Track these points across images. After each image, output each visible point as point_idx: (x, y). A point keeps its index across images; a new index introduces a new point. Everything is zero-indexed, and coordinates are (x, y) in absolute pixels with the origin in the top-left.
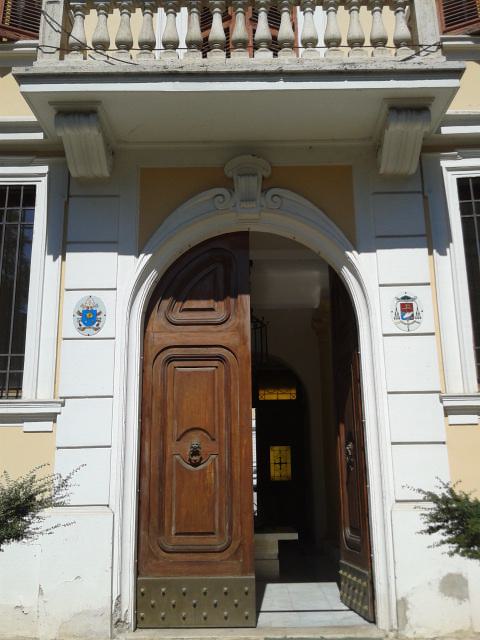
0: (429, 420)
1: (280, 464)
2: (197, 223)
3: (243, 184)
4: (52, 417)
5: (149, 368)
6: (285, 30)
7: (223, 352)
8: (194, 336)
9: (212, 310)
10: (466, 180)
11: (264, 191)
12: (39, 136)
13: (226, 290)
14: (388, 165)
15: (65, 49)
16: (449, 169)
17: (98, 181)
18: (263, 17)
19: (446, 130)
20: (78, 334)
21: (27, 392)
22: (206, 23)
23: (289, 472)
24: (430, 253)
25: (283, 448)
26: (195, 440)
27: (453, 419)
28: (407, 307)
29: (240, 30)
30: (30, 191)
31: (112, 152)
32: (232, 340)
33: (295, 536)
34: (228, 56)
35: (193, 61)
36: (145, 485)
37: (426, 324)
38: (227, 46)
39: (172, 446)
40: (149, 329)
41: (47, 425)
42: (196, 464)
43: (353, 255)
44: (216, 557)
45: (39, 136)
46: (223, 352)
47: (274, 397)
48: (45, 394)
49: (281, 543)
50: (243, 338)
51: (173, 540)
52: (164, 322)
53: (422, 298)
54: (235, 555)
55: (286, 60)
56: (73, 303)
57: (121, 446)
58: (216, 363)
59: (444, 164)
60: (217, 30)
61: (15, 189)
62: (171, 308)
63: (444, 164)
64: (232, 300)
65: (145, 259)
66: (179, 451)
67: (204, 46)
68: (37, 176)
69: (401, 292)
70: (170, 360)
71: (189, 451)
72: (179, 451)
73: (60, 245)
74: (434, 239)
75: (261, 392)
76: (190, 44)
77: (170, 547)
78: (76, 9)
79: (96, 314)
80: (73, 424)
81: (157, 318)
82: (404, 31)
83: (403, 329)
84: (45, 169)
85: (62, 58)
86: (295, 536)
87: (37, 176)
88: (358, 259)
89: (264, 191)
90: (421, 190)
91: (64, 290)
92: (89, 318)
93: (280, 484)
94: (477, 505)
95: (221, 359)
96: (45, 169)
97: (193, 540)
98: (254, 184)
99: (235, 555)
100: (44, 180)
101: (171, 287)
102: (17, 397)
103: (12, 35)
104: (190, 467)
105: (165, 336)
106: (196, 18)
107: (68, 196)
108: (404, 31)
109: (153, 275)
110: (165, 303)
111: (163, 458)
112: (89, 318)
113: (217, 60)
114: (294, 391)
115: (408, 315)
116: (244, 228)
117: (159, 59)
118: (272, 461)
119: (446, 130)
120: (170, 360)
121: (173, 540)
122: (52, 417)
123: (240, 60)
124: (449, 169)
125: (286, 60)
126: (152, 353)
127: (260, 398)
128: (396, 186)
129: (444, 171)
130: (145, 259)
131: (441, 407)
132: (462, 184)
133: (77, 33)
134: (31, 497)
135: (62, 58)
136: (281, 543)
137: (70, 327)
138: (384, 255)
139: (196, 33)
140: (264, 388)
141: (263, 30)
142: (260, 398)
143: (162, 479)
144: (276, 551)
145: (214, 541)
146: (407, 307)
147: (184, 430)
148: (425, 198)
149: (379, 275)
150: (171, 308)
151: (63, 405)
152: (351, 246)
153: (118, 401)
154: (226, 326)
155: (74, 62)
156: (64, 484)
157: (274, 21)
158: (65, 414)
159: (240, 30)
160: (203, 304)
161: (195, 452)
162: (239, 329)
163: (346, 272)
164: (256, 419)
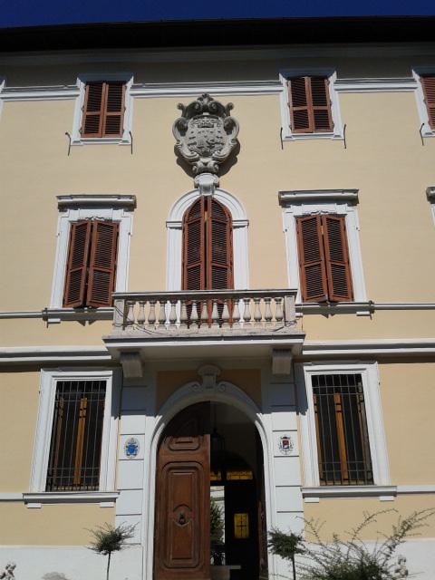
0: (294, 500)
1: (241, 526)
2: (185, 398)
3: (206, 379)
4: (114, 500)
5: (160, 474)
6: (226, 314)
7: (196, 465)
8: (182, 456)
9: (191, 442)
11: (217, 382)
12: (109, 357)
13: (197, 432)
14: (276, 370)
15: (126, 324)
16: (308, 371)
17: (138, 379)
18: (215, 307)
19: (305, 353)
20: (126, 458)
21: (101, 488)
23: (247, 533)
24: (298, 414)
25: (243, 515)
26: (182, 511)
27: (307, 499)
28: (286, 442)
29: (204, 315)
30: (104, 384)
31: (144, 365)
32: (200, 458)
33: (238, 567)
35: (180, 330)
36: (157, 536)
38: (199, 322)
39: (171, 514)
40: (160, 453)
41: (111, 504)
42: (182, 523)
43: (260, 415)
44: (191, 570)
45: (109, 357)
46: (196, 465)
47: (237, 478)
48: (110, 488)
49: (232, 571)
50: (207, 458)
51: (171, 562)
52: (167, 449)
53: (293, 438)
54: (201, 570)
55: (226, 330)
56: (124, 441)
59: (305, 368)
60: (194, 315)
61: (96, 383)
62: (171, 441)
63: (305, 368)
64: (201, 437)
65: (159, 418)
66: (174, 517)
67: (188, 322)
68: (107, 376)
69: (283, 434)
70: (170, 469)
71: (179, 516)
72: (174, 517)
73: (118, 412)
74: (300, 408)
75: (228, 474)
76: (182, 321)
77: (170, 566)
78: (130, 304)
80: (123, 503)
81: (164, 446)
83: (283, 453)
84: (111, 372)
85: (124, 329)
86: (238, 567)
87: (107, 376)
88: (263, 417)
89: (217, 382)
90: (292, 381)
91: (120, 435)
92: (132, 449)
93: (242, 540)
95: (195, 468)
96: (111, 372)
97: (181, 562)
98: (212, 379)
99: (201, 570)
100: (111, 378)
101: (170, 432)
102: (95, 490)
103: (96, 305)
104: (179, 525)
105: (165, 458)
106: (184, 308)
107: (122, 386)
108: (280, 314)
109: (163, 425)
110: (168, 439)
111: (166, 522)
112: (132, 449)
113: (194, 328)
114: (251, 473)
115: (286, 446)
116: (208, 400)
117: (168, 330)
118: (235, 524)
119: (305, 353)
121: (171, 562)
122: (114, 500)
123: (204, 330)
124: (308, 371)
125: (226, 330)
126: (161, 466)
127: (228, 478)
128: (281, 380)
129: (305, 373)
130: (159, 418)
131: (301, 493)
132: (314, 378)
133: (130, 317)
134: (120, 534)
135: (124, 329)
136: (232, 571)
138: (274, 415)
140: (231, 470)
141: (215, 314)
142: (228, 478)
143: (166, 532)
144: (228, 577)
145: (190, 562)
146: (286, 442)
147: (177, 505)
148: (295, 386)
149: (273, 425)
150: (171, 441)
151: (119, 493)
152: (257, 409)
153: (145, 491)
154: (199, 450)
155: (131, 332)
156: (133, 529)
157: (231, 310)
158: (120, 498)
159: (204, 315)
160: (187, 439)
161: (182, 517)
162: (205, 452)
163: (257, 423)
164: (240, 480)
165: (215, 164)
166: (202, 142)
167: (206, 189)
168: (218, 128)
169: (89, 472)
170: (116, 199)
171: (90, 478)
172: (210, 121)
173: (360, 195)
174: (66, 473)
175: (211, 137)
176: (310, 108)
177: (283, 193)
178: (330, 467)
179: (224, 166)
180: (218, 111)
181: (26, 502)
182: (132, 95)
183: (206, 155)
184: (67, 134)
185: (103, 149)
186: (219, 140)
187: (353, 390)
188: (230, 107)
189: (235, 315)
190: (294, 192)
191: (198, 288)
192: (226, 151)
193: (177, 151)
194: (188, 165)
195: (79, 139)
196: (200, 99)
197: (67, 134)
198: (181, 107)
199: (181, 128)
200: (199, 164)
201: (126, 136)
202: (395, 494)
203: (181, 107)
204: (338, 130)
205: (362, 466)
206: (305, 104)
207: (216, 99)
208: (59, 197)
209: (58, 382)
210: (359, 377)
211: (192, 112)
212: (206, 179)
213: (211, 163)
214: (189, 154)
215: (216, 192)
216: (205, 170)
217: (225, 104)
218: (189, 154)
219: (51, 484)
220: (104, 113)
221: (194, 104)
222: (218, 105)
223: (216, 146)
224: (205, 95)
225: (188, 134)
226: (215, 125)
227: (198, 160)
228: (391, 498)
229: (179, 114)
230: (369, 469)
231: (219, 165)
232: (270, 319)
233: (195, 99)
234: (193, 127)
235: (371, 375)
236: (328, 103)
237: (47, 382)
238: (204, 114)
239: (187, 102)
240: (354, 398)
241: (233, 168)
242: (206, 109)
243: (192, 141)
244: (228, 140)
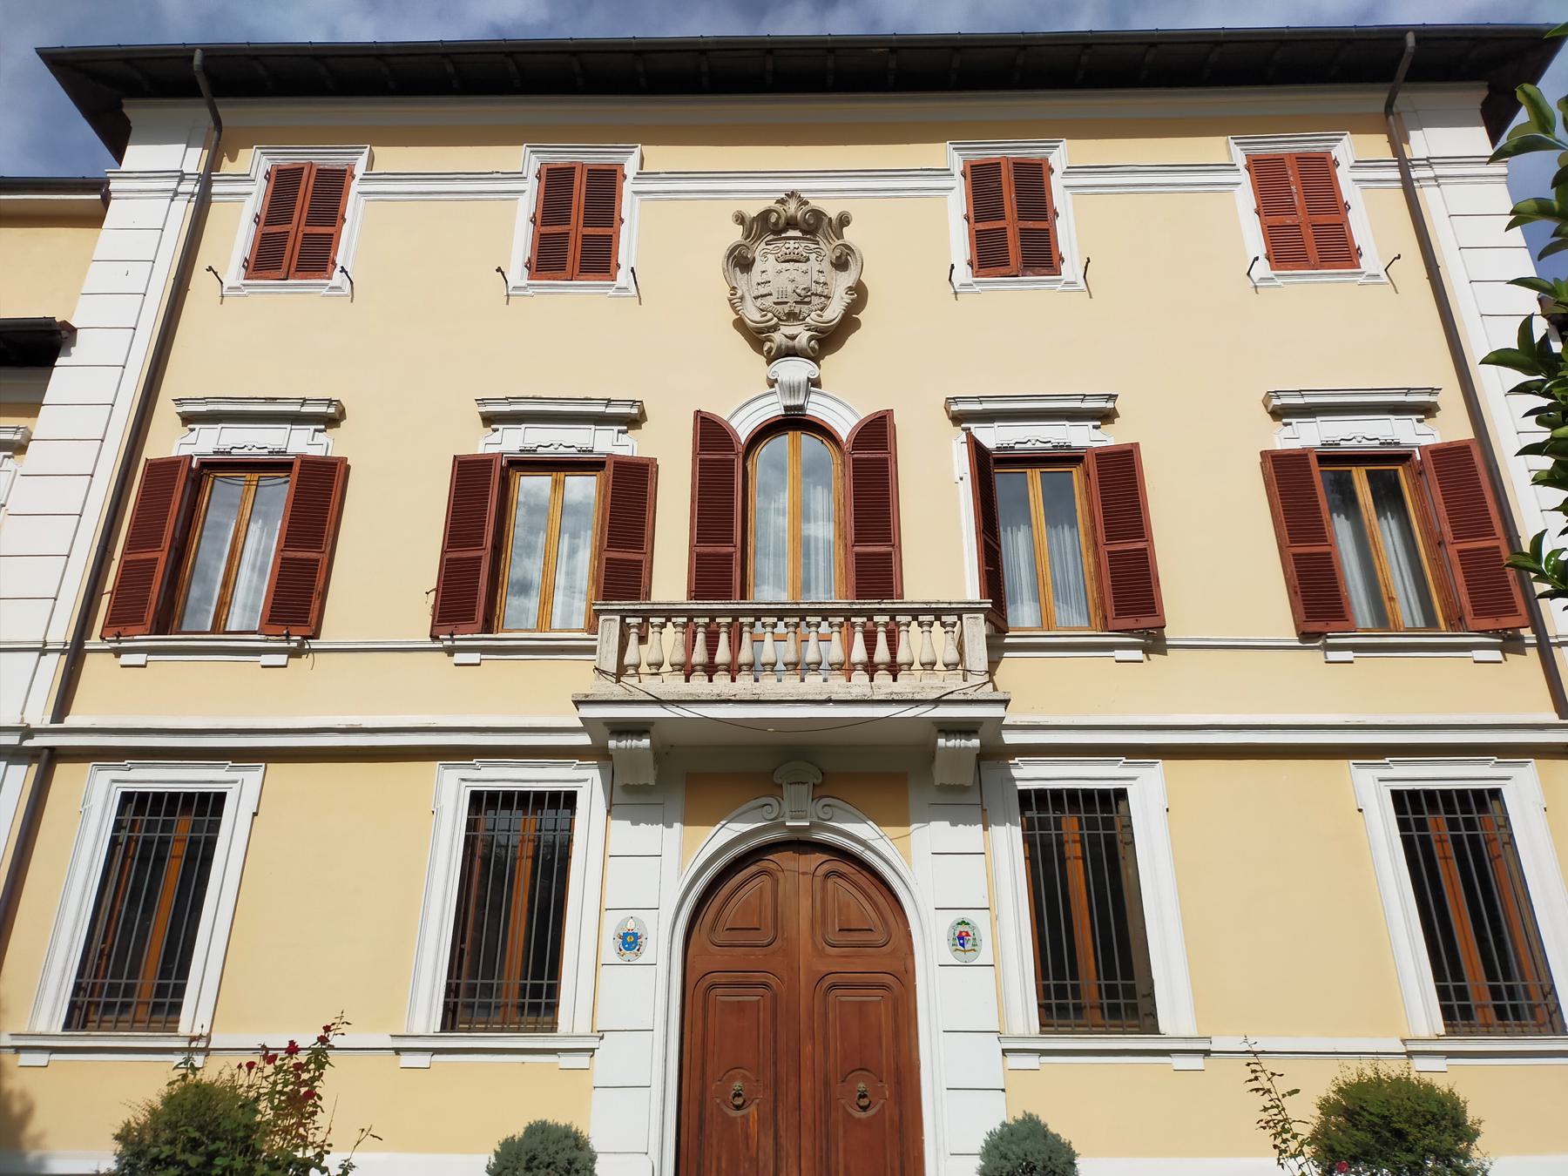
0: (984, 1061)
7: (888, 979)
10: (1401, 792)
18: (859, 638)
22: (690, 647)
27: (1015, 1061)
28: (963, 939)
34: (733, 680)
35: (673, 685)
37: (985, 956)
41: (581, 1061)
56: (613, 924)
57: (660, 1088)
58: (761, 991)
67: (687, 670)
70: (833, 987)
79: (636, 937)
82: (953, 656)
92: (630, 942)
94: (592, 1171)
95: (884, 986)
108: (953, 656)
112: (630, 942)
113: (722, 684)
120: (833, 987)
123: (813, 685)
137: (610, 951)
139: (679, 657)
157: (735, 645)
158: (603, 1048)
165: (811, 339)
166: (783, 293)
167: (792, 390)
168: (817, 267)
169: (536, 991)
170: (601, 409)
171: (537, 1001)
172: (801, 247)
173: (1119, 405)
174: (487, 990)
175: (804, 282)
176: (1011, 223)
177: (955, 400)
178: (1061, 992)
179: (828, 340)
180: (813, 225)
181: (398, 1051)
182: (636, 193)
183: (792, 316)
184: (499, 270)
185: (575, 299)
186: (819, 289)
187: (1109, 824)
188: (844, 220)
189: (902, 657)
190: (980, 399)
191: (727, 596)
192: (834, 312)
193: (740, 324)
194: (756, 337)
195: (524, 282)
196: (781, 202)
197: (499, 270)
198: (740, 219)
199: (741, 261)
200: (778, 337)
201: (623, 277)
202: (1207, 1053)
203: (740, 219)
204: (1071, 269)
205: (1130, 992)
206: (1002, 218)
207: (814, 204)
208: (482, 401)
209: (473, 793)
210: (1121, 794)
211: (765, 226)
212: (795, 370)
213: (803, 338)
214: (757, 317)
215: (813, 397)
216: (791, 352)
217: (833, 212)
218: (757, 317)
219: (451, 1020)
220: (577, 228)
221: (766, 214)
222: (818, 214)
223: (815, 300)
224: (792, 195)
225: (757, 268)
226: (813, 257)
227: (775, 328)
228: (1197, 1062)
229: (736, 234)
230: (1125, 822)
231: (819, 341)
232: (659, 665)
233: (771, 204)
234: (767, 260)
235: (1150, 794)
236: (1050, 215)
237: (450, 790)
238: (791, 233)
239: (753, 210)
240: (1111, 842)
241: (853, 340)
242: (791, 223)
243: (762, 290)
244: (841, 284)
